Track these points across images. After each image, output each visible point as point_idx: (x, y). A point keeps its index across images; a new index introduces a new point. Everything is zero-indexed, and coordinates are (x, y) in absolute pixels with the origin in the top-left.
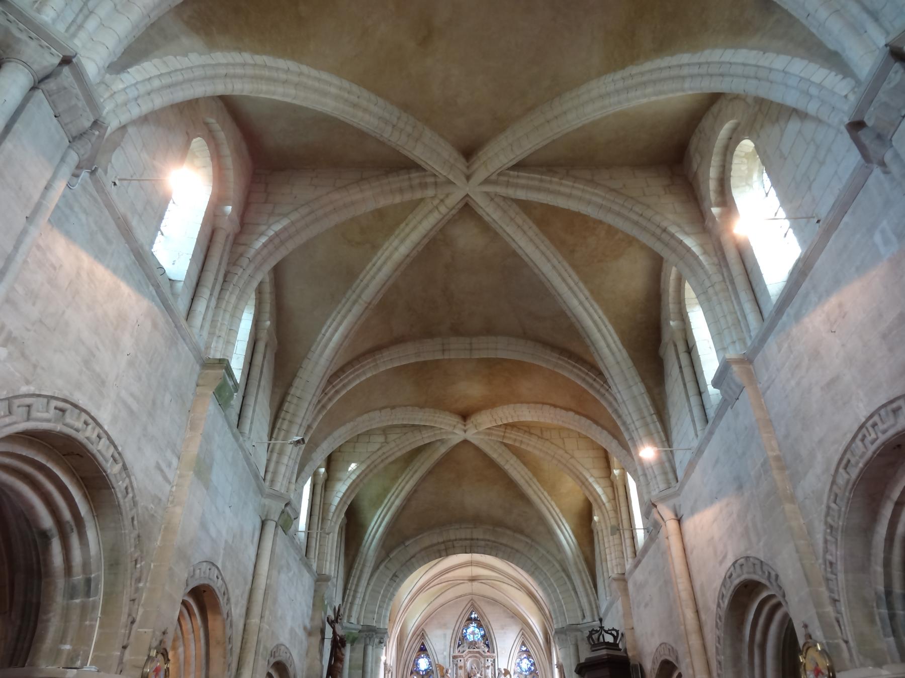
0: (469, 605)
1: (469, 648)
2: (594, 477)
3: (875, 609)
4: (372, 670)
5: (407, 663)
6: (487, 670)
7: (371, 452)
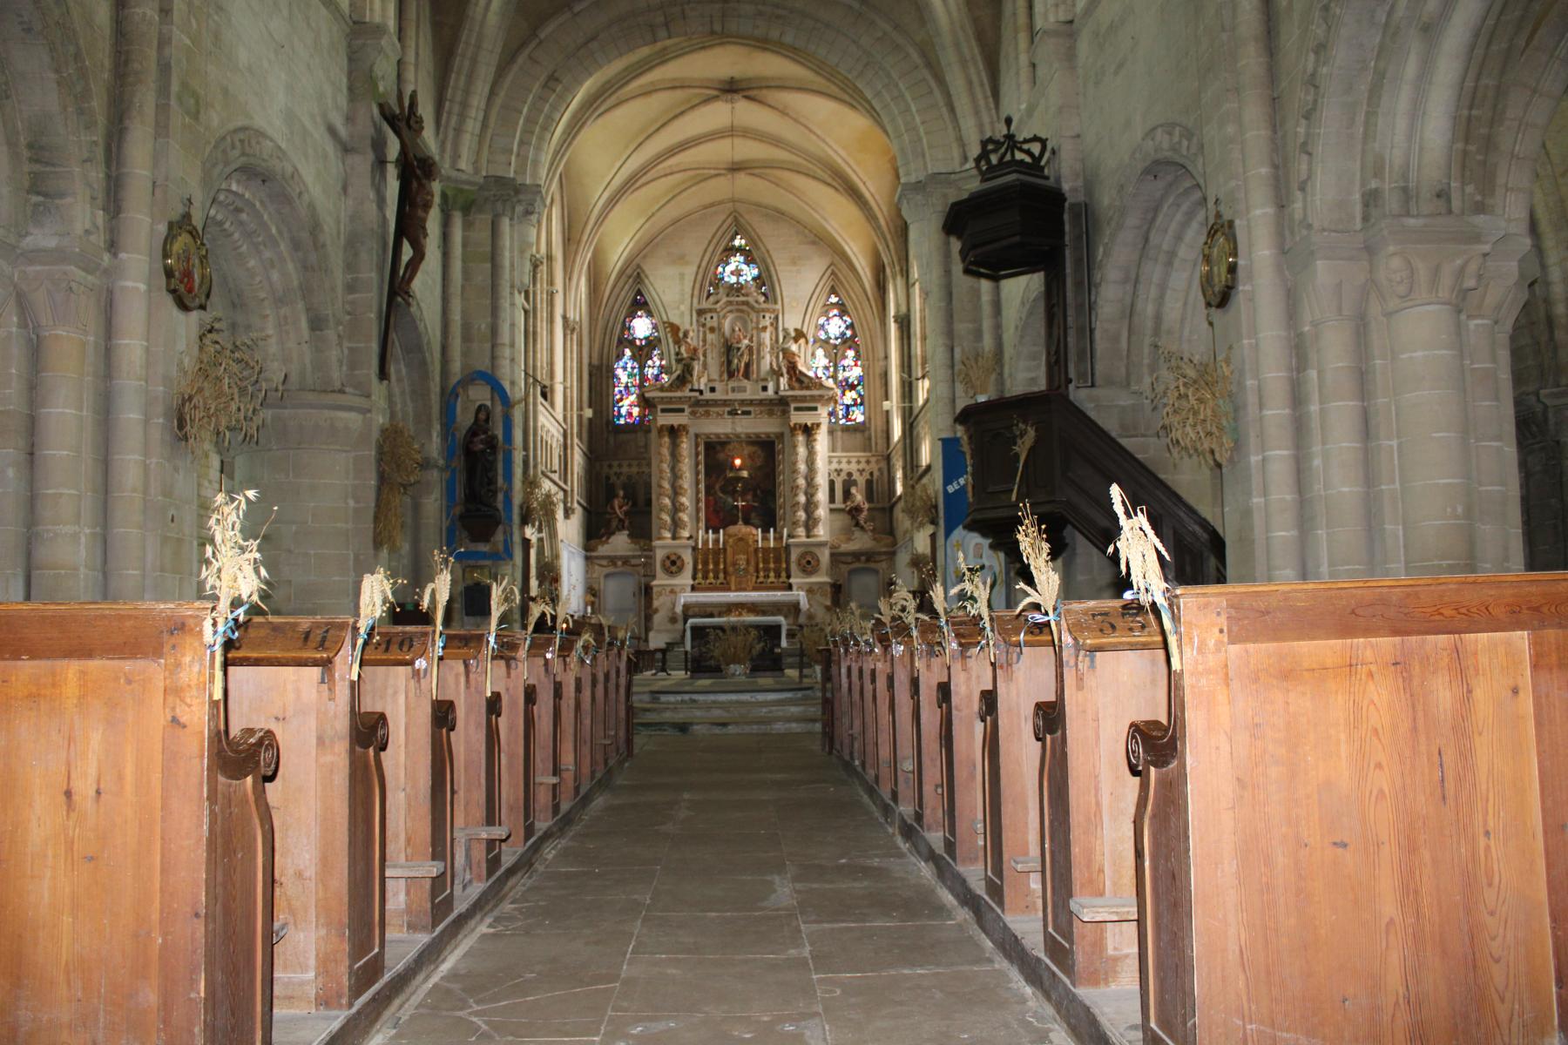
0: (729, 221)
4: (512, 265)
5: (610, 325)
6: (763, 335)
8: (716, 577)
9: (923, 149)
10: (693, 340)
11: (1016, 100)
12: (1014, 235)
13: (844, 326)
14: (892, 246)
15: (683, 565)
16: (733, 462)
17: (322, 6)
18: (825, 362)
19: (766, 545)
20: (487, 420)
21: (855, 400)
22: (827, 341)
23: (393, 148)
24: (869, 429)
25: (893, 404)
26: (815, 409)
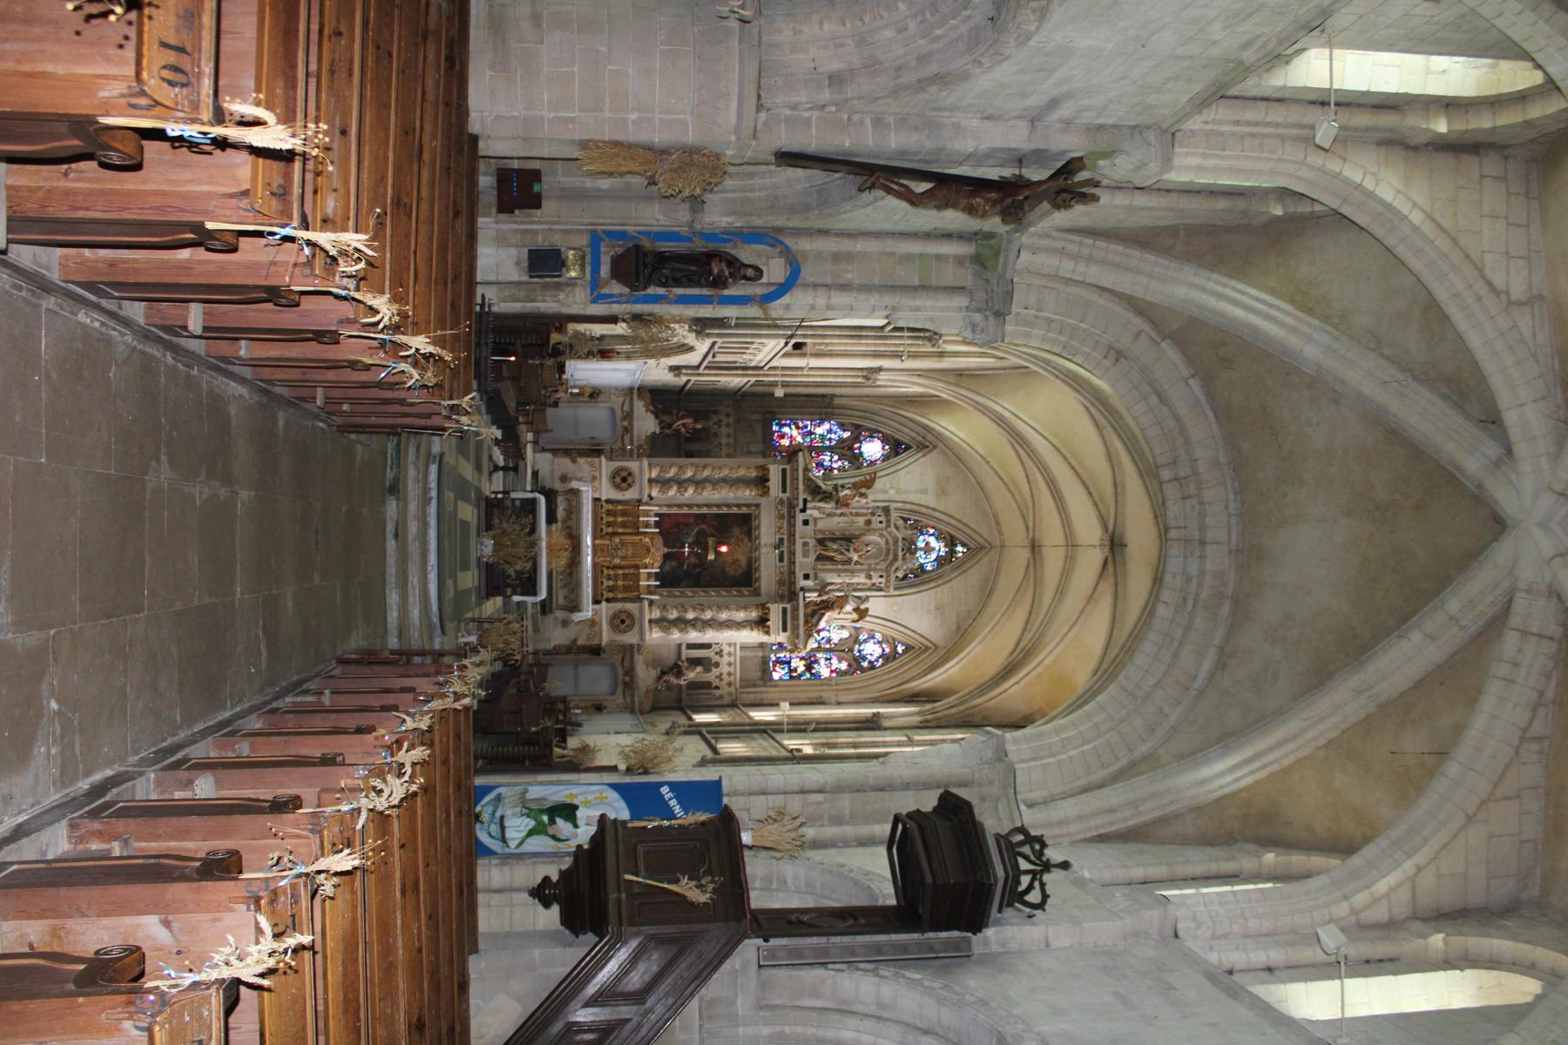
0: (981, 541)
2: (1416, 875)
3: (565, 752)
6: (863, 575)
7: (1483, 265)
8: (609, 524)
9: (1043, 758)
10: (857, 502)
11: (1091, 865)
12: (933, 876)
13: (873, 659)
14: (953, 711)
15: (622, 490)
16: (724, 544)
17: (1189, 96)
18: (835, 640)
19: (643, 577)
20: (745, 278)
21: (795, 670)
22: (856, 641)
23: (1035, 174)
24: (765, 686)
25: (784, 712)
26: (785, 630)
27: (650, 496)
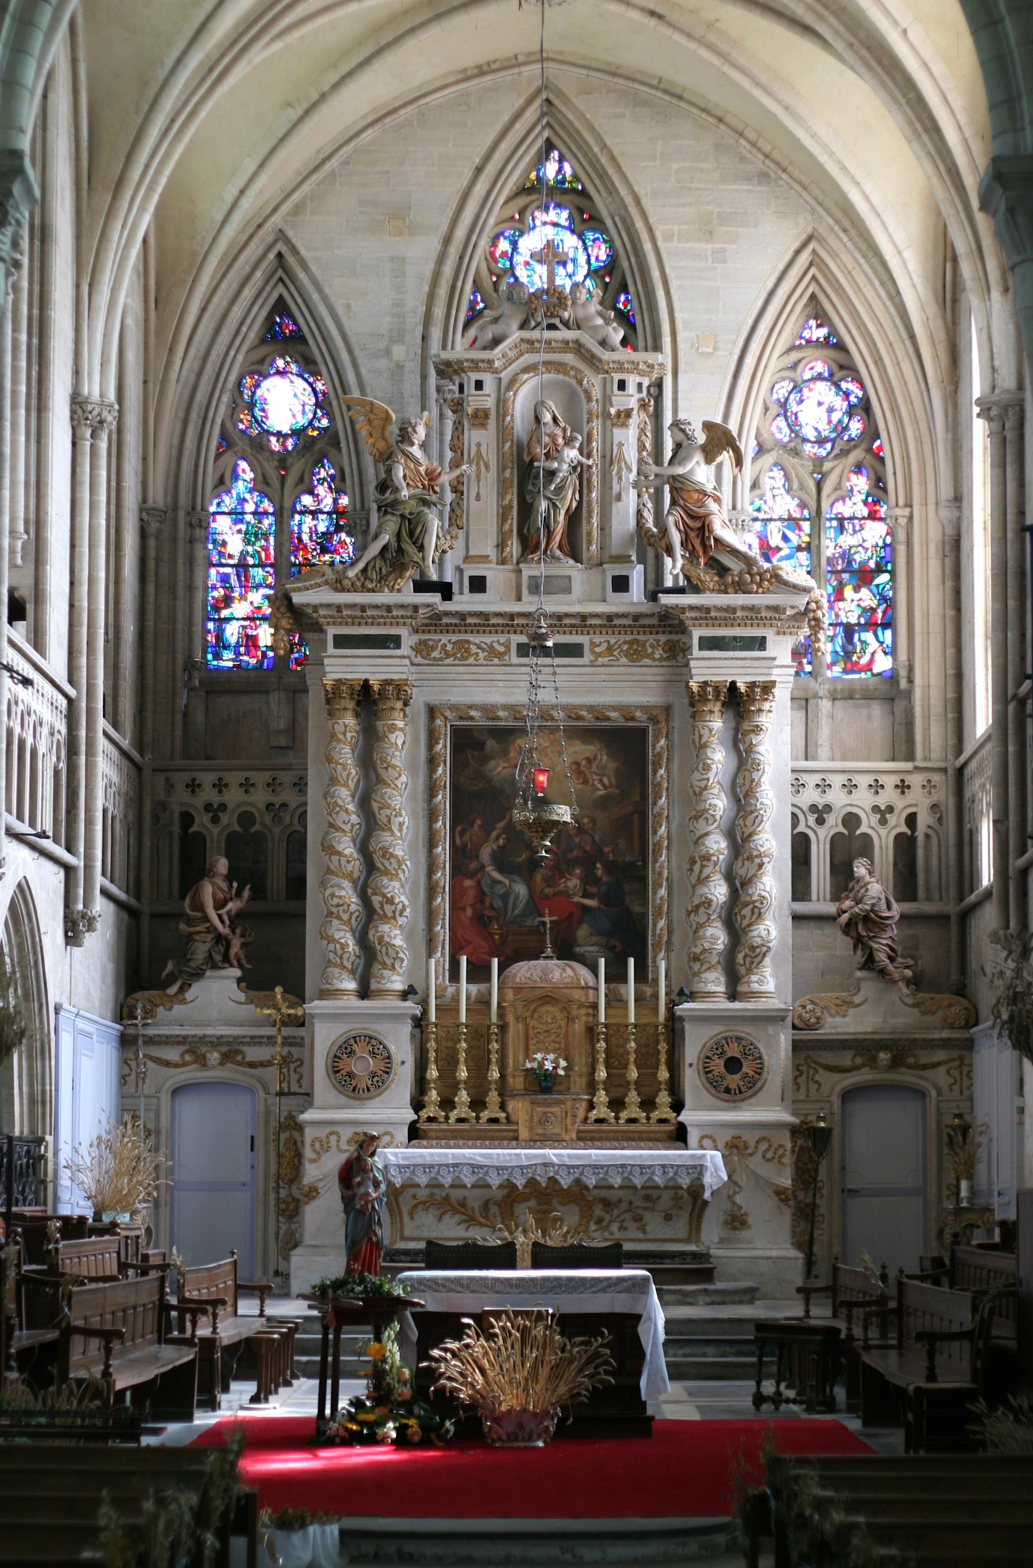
0: (532, 114)
1: (523, 326)
6: (618, 434)
24: (909, 694)
26: (760, 643)
27: (405, 995)
